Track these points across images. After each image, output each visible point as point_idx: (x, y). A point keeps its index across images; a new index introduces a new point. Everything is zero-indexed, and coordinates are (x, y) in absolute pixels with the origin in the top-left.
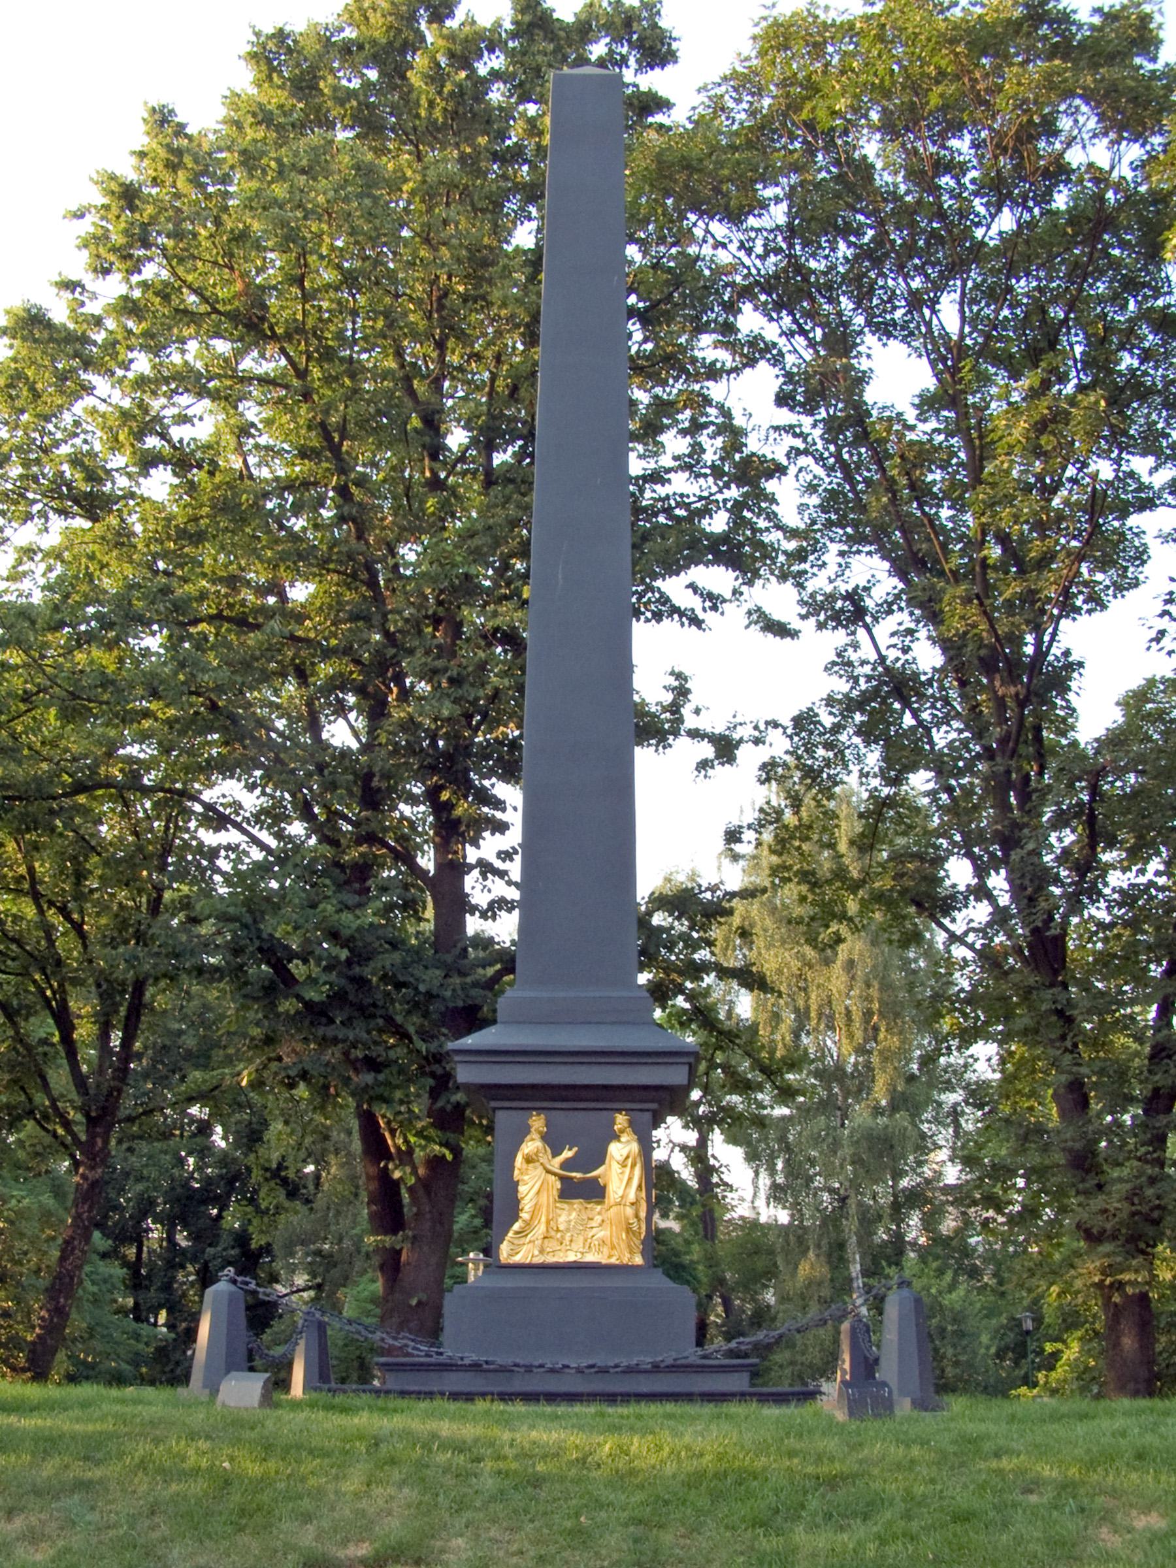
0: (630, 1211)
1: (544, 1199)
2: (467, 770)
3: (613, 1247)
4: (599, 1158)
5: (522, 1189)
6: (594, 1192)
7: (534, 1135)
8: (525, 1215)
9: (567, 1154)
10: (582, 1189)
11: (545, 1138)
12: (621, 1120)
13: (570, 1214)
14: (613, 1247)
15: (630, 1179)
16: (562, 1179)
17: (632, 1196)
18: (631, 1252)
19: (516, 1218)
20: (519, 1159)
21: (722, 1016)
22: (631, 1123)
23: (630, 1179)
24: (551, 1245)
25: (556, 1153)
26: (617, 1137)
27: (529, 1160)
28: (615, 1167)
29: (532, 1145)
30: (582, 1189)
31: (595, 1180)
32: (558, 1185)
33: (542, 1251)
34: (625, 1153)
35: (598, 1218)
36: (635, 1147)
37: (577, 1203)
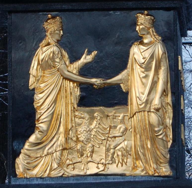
0: (154, 118)
1: (61, 108)
2: (185, 178)
3: (137, 158)
4: (121, 62)
5: (39, 97)
6: (117, 97)
7: (49, 39)
8: (43, 126)
9: (86, 59)
10: (100, 95)
11: (60, 43)
12: (143, 20)
13: (89, 124)
14: (137, 158)
15: (154, 84)
16: (80, 85)
17: (156, 102)
18: (157, 162)
19: (32, 129)
20: (34, 63)
21: (177, 13)
22: (154, 24)
23: (154, 84)
24: (69, 158)
25: (74, 58)
26: (139, 40)
27: (46, 65)
28: (138, 71)
29: (44, 52)
30: (100, 95)
31: (117, 86)
32: (77, 92)
33: (60, 165)
34: (147, 55)
35: (121, 127)
36: (159, 49)
37: (98, 111)
